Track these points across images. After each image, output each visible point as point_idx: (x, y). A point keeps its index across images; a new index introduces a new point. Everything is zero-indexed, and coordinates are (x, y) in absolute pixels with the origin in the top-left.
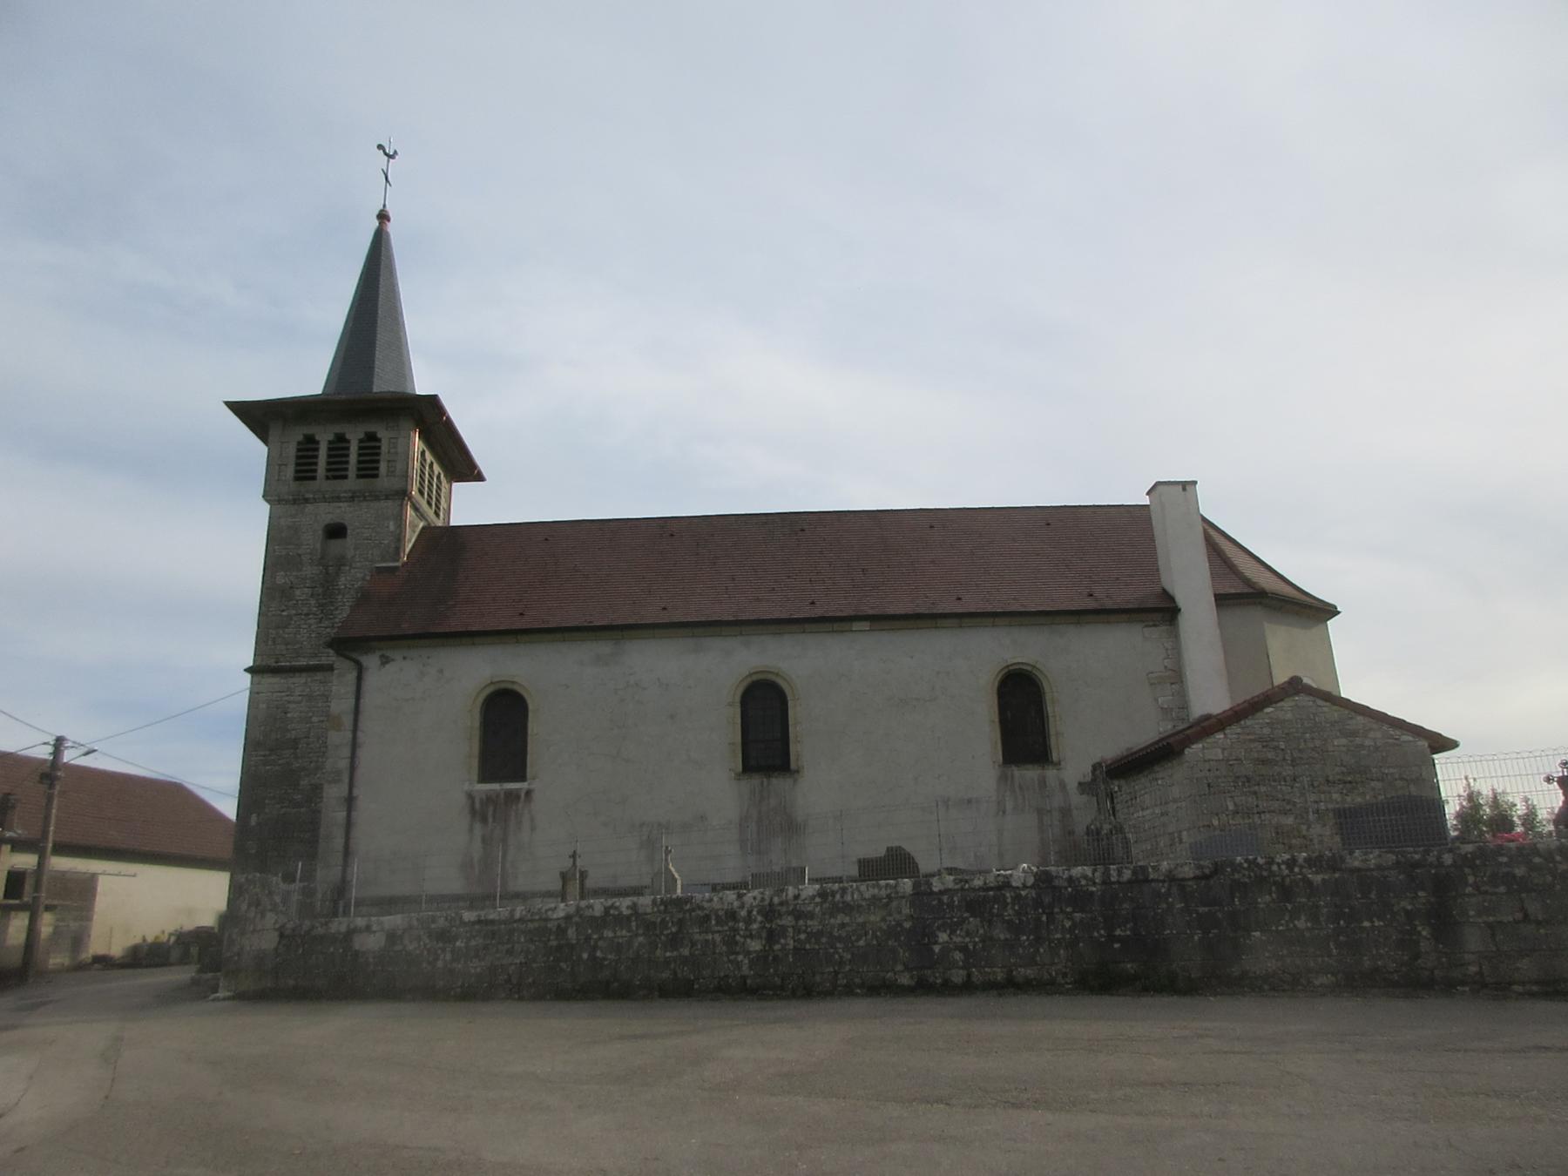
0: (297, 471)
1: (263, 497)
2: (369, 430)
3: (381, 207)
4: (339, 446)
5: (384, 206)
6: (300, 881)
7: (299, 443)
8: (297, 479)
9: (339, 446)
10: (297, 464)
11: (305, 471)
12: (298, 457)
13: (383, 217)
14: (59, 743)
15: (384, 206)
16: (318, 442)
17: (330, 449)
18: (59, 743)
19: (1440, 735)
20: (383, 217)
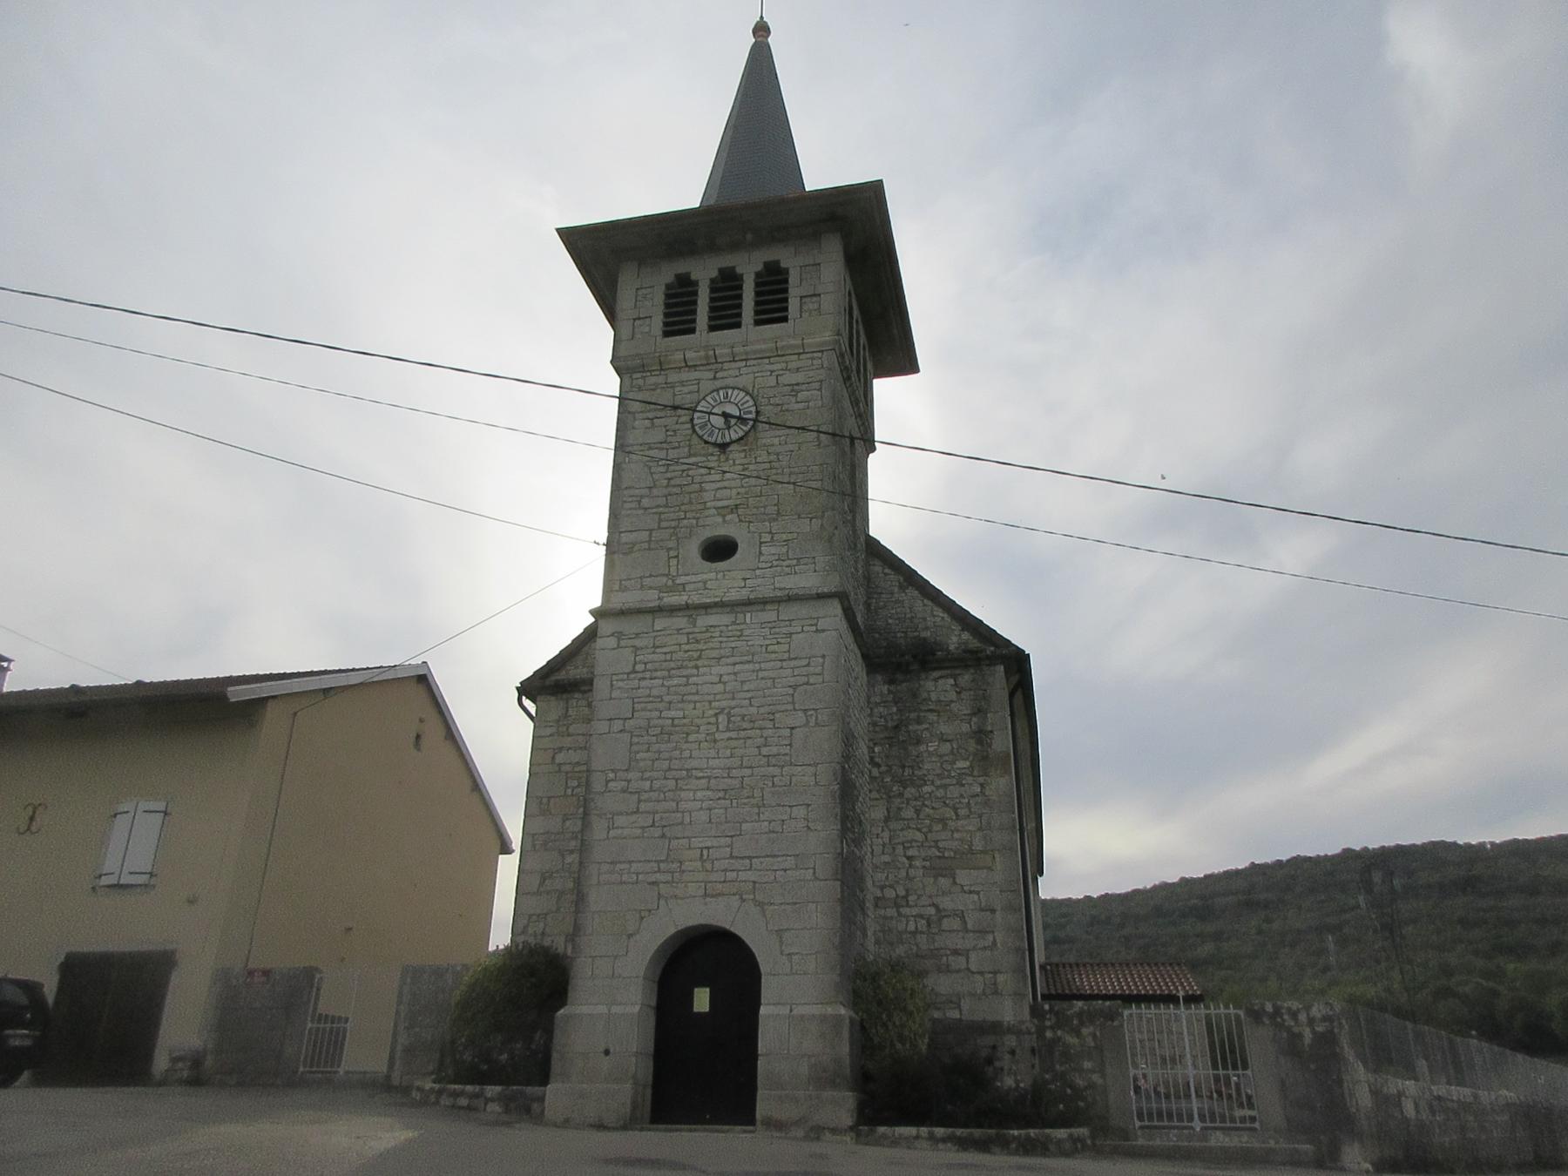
0: (666, 324)
1: (611, 362)
2: (680, 272)
3: (758, 19)
4: (728, 284)
5: (762, 17)
6: (1213, 1074)
7: (668, 287)
8: (667, 334)
9: (728, 284)
10: (666, 315)
11: (678, 320)
12: (667, 306)
13: (761, 30)
14: (497, 946)
15: (762, 17)
16: (786, 271)
17: (757, 285)
18: (497, 946)
19: (879, 542)
20: (761, 30)
